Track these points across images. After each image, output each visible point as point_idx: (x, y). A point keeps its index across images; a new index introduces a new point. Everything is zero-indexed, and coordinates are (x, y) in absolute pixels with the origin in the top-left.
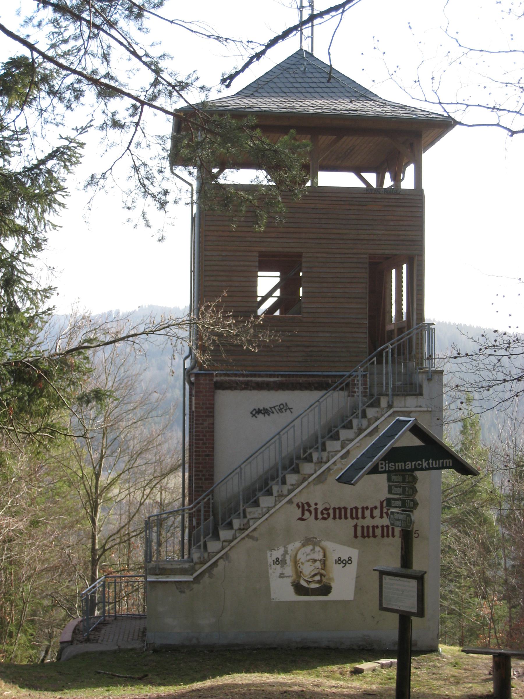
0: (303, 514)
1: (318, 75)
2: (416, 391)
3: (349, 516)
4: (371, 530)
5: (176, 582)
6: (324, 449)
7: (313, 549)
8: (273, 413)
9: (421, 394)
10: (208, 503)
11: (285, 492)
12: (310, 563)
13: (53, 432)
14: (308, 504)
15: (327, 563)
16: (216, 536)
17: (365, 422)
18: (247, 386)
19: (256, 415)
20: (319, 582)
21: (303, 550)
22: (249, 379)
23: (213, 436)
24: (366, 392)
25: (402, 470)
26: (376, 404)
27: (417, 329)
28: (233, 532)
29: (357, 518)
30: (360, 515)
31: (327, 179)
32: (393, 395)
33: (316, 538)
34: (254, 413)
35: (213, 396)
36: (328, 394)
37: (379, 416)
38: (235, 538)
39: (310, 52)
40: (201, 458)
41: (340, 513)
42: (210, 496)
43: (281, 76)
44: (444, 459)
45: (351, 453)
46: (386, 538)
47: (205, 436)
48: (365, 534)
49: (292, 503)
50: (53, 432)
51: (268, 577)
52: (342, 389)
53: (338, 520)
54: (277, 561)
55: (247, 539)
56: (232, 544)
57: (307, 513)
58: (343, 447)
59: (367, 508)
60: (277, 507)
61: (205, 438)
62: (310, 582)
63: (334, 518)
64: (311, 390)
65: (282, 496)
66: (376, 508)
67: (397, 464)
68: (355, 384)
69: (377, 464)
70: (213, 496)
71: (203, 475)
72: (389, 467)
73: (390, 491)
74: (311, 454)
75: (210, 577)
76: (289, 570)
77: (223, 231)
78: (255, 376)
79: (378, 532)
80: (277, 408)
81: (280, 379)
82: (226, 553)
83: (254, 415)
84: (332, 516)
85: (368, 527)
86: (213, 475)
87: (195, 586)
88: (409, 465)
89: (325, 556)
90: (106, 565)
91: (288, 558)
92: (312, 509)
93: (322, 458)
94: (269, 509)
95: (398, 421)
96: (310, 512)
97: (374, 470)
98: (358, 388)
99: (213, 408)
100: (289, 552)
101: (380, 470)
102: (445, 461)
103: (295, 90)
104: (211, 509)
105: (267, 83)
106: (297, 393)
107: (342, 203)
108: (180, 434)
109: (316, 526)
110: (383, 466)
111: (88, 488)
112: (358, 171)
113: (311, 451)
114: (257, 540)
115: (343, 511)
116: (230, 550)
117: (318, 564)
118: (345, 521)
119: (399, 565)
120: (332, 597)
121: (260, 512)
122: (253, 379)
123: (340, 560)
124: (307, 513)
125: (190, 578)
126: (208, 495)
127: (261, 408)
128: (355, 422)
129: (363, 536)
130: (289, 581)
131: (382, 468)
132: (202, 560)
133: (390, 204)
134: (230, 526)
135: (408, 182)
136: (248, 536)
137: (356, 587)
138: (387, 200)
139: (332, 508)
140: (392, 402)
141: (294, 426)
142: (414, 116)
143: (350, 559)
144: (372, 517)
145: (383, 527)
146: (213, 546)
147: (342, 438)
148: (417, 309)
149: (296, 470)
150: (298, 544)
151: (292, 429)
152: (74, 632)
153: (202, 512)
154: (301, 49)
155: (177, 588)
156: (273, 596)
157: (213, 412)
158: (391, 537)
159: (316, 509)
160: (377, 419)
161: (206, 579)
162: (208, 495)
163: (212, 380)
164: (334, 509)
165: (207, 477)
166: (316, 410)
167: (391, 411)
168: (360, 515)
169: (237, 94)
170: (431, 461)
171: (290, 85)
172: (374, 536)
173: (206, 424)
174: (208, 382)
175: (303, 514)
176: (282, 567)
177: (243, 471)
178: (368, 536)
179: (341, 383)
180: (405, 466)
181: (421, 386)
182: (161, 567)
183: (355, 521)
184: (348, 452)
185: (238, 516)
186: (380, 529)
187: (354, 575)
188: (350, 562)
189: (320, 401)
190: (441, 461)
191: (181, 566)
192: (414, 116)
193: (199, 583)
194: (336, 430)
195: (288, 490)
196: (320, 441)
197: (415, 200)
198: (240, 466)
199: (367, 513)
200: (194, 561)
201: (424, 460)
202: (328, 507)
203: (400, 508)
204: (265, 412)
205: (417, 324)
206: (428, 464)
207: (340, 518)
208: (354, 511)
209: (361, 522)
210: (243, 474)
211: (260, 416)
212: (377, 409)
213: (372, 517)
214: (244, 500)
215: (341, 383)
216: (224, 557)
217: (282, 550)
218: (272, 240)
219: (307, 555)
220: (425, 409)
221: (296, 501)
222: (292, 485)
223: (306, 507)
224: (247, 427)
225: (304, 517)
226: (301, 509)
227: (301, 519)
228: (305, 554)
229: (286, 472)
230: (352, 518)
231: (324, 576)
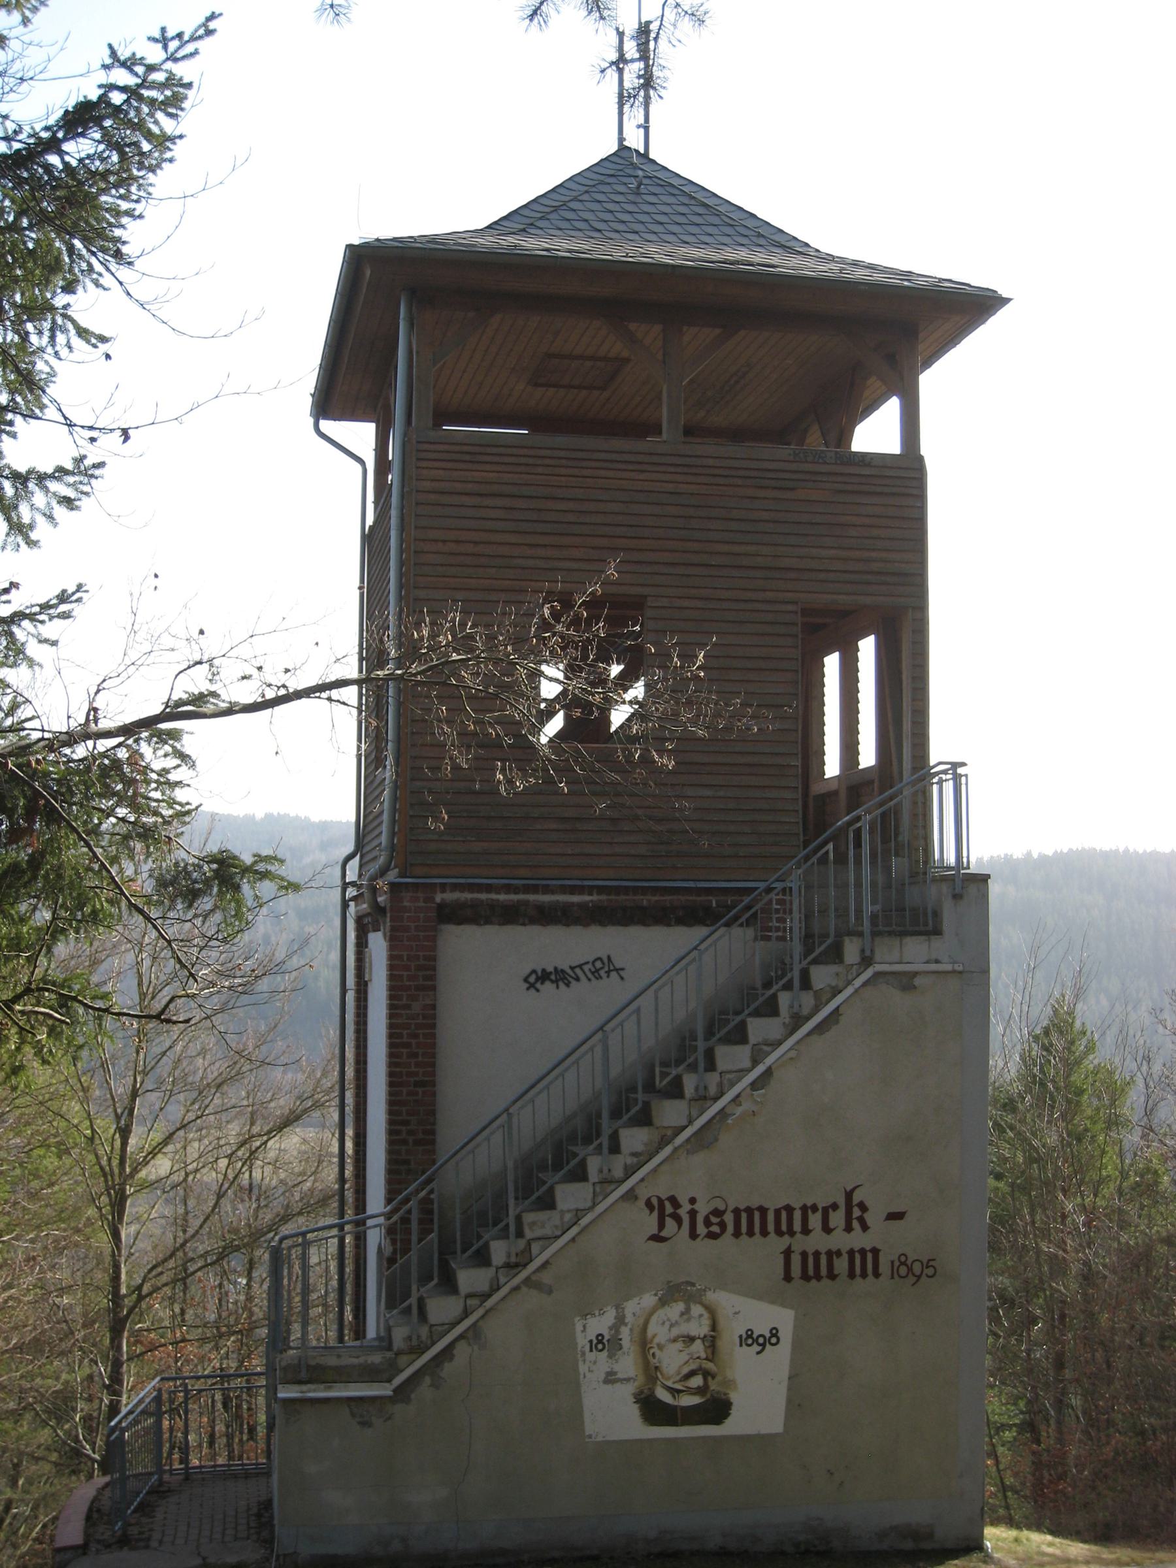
0: (661, 1225)
1: (671, 200)
2: (926, 924)
3: (771, 1227)
4: (823, 1260)
5: (350, 1399)
6: (711, 1066)
7: (686, 1312)
8: (578, 979)
9: (937, 932)
11: (618, 1173)
12: (679, 1345)
13: (64, 1002)
14: (673, 1200)
15: (719, 1343)
16: (449, 1284)
17: (807, 1000)
18: (510, 915)
19: (538, 985)
20: (700, 1391)
21: (661, 1314)
22: (521, 897)
23: (433, 1036)
26: (835, 954)
28: (491, 1272)
29: (792, 1233)
30: (797, 1226)
32: (875, 934)
33: (693, 1285)
34: (532, 979)
35: (434, 939)
37: (841, 985)
38: (495, 1287)
39: (642, 151)
40: (405, 1090)
41: (751, 1221)
43: (585, 197)
45: (776, 1074)
46: (859, 1280)
47: (416, 1036)
48: (811, 1272)
49: (636, 1198)
50: (64, 1002)
51: (578, 1385)
52: (748, 923)
53: (744, 1237)
54: (600, 1342)
55: (524, 1289)
56: (489, 1303)
57: (670, 1223)
58: (755, 1062)
59: (814, 1208)
60: (600, 1209)
61: (414, 1041)
62: (679, 1391)
63: (737, 1234)
64: (669, 925)
65: (609, 1182)
66: (835, 1207)
71: (410, 1133)
75: (435, 1386)
76: (628, 1364)
77: (457, 542)
78: (534, 889)
79: (841, 1265)
80: (586, 968)
81: (595, 897)
82: (474, 1324)
83: (532, 986)
84: (730, 1228)
85: (817, 1254)
86: (433, 1132)
87: (398, 1408)
89: (714, 1327)
90: (141, 1330)
91: (625, 1332)
92: (683, 1213)
93: (706, 1088)
94: (579, 1214)
96: (678, 1220)
100: (629, 1318)
103: (621, 227)
105: (556, 209)
106: (635, 931)
107: (740, 482)
108: (334, 1033)
109: (691, 1254)
111: (104, 1162)
114: (550, 1292)
115: (757, 1215)
116: (483, 1317)
117: (698, 1348)
118: (763, 1239)
120: (731, 1426)
121: (558, 1222)
122: (531, 897)
123: (750, 1336)
124: (670, 1223)
125: (385, 1390)
127: (550, 969)
128: (784, 999)
129: (805, 1277)
130: (626, 1392)
132: (415, 1342)
133: (849, 488)
134: (482, 1258)
136: (527, 1281)
137: (789, 1401)
138: (840, 479)
139: (731, 1208)
140: (872, 951)
141: (638, 1010)
142: (906, 283)
143: (774, 1333)
144: (827, 1229)
145: (851, 1253)
146: (441, 1308)
147: (753, 1038)
148: (913, 734)
149: (645, 1119)
150: (649, 1300)
151: (634, 1017)
152: (88, 1518)
154: (623, 148)
155: (353, 1415)
156: (589, 1428)
157: (432, 978)
158: (871, 1276)
159: (693, 1214)
160: (836, 992)
161: (425, 1390)
163: (432, 900)
164: (737, 1212)
165: (421, 1136)
167: (869, 973)
168: (797, 1226)
169: (489, 227)
171: (608, 216)
172: (832, 1276)
173: (416, 1007)
174: (421, 904)
175: (661, 1225)
176: (610, 1356)
177: (515, 1120)
178: (818, 1277)
179: (748, 908)
181: (936, 914)
182: (313, 1363)
183: (786, 1239)
184: (768, 1072)
185: (504, 1235)
186: (845, 1256)
187: (785, 1372)
188: (774, 1340)
189: (702, 947)
191: (361, 1360)
192: (906, 283)
193: (407, 1400)
194: (739, 1018)
195: (626, 1167)
196: (701, 1045)
198: (507, 1110)
199: (815, 1220)
200: (395, 1348)
202: (722, 1207)
204: (559, 977)
207: (751, 1233)
208: (784, 1215)
209: (800, 1243)
211: (548, 987)
212: (833, 969)
213: (827, 1229)
214: (516, 1190)
216: (470, 1334)
217: (610, 1316)
218: (574, 565)
219: (672, 1325)
220: (949, 967)
221: (644, 1193)
222: (634, 1154)
223: (669, 1209)
224: (531, 1014)
225: (663, 1234)
226: (655, 1213)
228: (667, 1324)
230: (779, 1233)
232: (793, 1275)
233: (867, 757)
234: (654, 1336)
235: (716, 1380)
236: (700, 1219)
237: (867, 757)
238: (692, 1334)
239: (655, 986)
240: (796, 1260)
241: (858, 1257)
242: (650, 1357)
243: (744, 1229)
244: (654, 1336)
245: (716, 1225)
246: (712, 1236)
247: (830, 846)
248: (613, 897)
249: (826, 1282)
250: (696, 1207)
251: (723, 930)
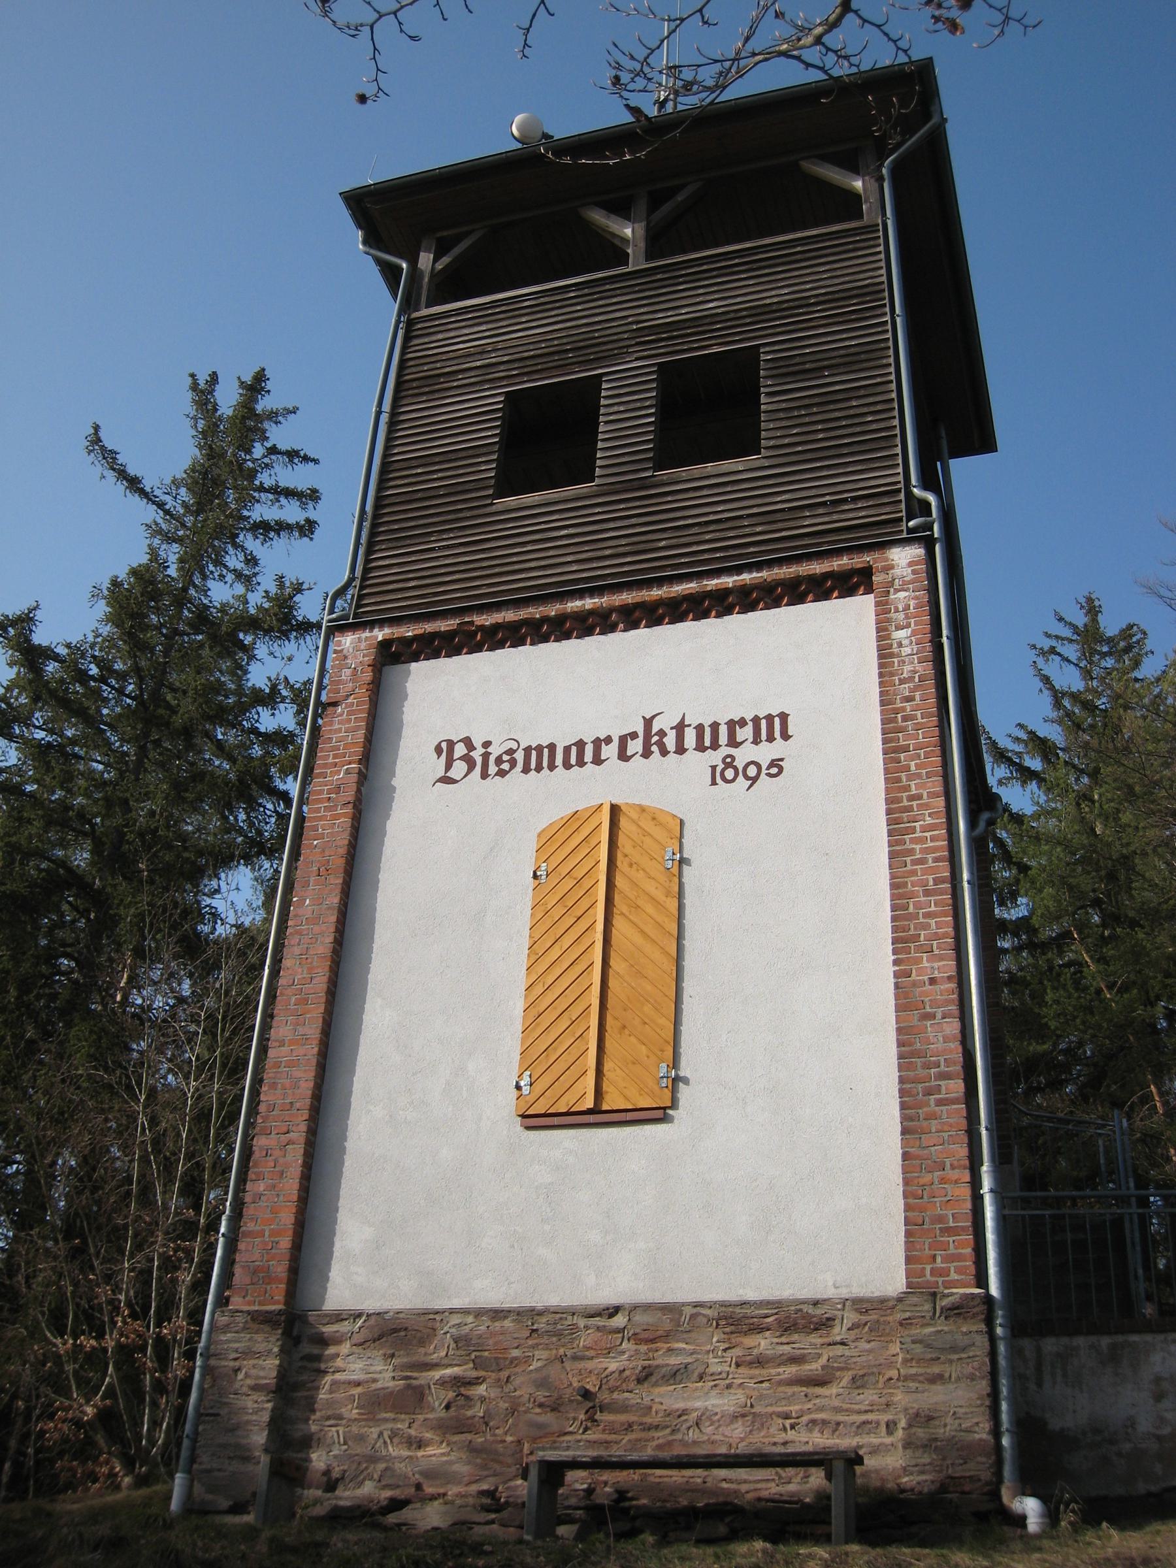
0: (449, 766)
14: (468, 742)
53: (533, 773)
63: (526, 770)
66: (634, 735)
92: (477, 755)
119: (855, 613)
139: (522, 747)
145: (756, 720)
159: (486, 756)
175: (449, 766)
186: (750, 724)
227: (446, 780)
230: (700, 747)
241: (764, 723)
248: (755, 575)
250: (489, 750)
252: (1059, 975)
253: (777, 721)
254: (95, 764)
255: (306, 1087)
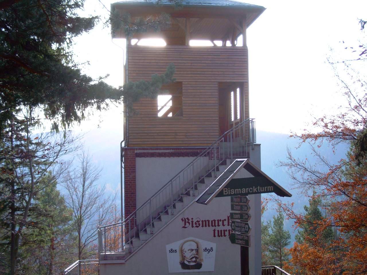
0: (185, 224)
2: (246, 156)
4: (223, 232)
10: (133, 219)
12: (190, 251)
14: (188, 219)
20: (194, 262)
23: (135, 183)
24: (218, 157)
25: (239, 194)
27: (246, 122)
29: (215, 226)
30: (217, 224)
31: (194, 43)
35: (135, 161)
36: (197, 159)
40: (129, 195)
41: (206, 223)
42: (134, 216)
44: (267, 186)
52: (205, 156)
53: (204, 227)
57: (187, 224)
59: (220, 220)
61: (131, 184)
62: (190, 262)
63: (203, 226)
64: (189, 157)
66: (225, 220)
67: (236, 190)
68: (213, 153)
69: (222, 190)
70: (135, 215)
71: (130, 204)
72: (230, 192)
73: (232, 209)
74: (189, 191)
78: (157, 149)
81: (171, 151)
84: (201, 225)
88: (244, 191)
92: (190, 221)
95: (237, 161)
96: (189, 223)
97: (220, 194)
98: (214, 155)
99: (135, 167)
101: (224, 194)
102: (268, 187)
104: (134, 223)
110: (227, 191)
112: (212, 39)
113: (189, 190)
117: (194, 252)
123: (206, 249)
124: (187, 224)
126: (133, 215)
129: (219, 236)
131: (226, 193)
135: (239, 42)
139: (201, 220)
141: (179, 176)
143: (212, 248)
151: (179, 178)
153: (130, 225)
159: (192, 222)
162: (133, 215)
163: (134, 152)
164: (202, 221)
166: (192, 167)
168: (217, 224)
170: (259, 188)
172: (225, 236)
175: (185, 224)
177: (152, 202)
179: (205, 153)
180: (241, 191)
181: (248, 153)
183: (214, 228)
186: (222, 221)
188: (212, 250)
189: (194, 162)
190: (266, 188)
194: (202, 178)
197: (243, 52)
199: (221, 223)
201: (254, 187)
203: (239, 219)
205: (245, 119)
206: (257, 190)
207: (206, 226)
208: (213, 222)
209: (217, 228)
210: (152, 203)
213: (224, 225)
215: (205, 153)
223: (187, 221)
226: (184, 222)
227: (184, 227)
229: (176, 201)
230: (212, 226)
231: (198, 258)
232: (216, 235)
233: (239, 117)
234: (184, 249)
235: (199, 259)
236: (194, 223)
237: (239, 117)
238: (193, 249)
239: (184, 171)
240: (216, 232)
242: (183, 254)
243: (204, 225)
244: (184, 249)
245: (197, 224)
246: (197, 227)
247: (223, 138)
248: (175, 151)
249: (223, 237)
250: (193, 220)
251: (200, 157)
252: (326, 266)
253: (207, 222)
254: (40, 191)
255: (121, 209)
